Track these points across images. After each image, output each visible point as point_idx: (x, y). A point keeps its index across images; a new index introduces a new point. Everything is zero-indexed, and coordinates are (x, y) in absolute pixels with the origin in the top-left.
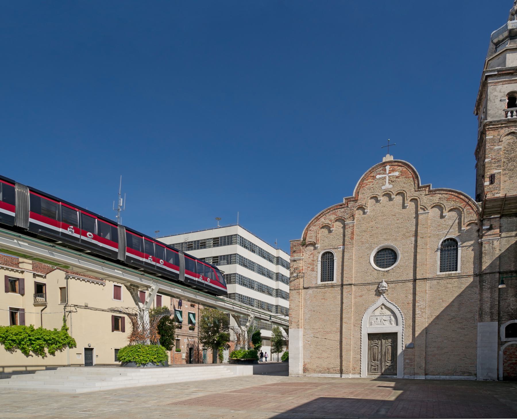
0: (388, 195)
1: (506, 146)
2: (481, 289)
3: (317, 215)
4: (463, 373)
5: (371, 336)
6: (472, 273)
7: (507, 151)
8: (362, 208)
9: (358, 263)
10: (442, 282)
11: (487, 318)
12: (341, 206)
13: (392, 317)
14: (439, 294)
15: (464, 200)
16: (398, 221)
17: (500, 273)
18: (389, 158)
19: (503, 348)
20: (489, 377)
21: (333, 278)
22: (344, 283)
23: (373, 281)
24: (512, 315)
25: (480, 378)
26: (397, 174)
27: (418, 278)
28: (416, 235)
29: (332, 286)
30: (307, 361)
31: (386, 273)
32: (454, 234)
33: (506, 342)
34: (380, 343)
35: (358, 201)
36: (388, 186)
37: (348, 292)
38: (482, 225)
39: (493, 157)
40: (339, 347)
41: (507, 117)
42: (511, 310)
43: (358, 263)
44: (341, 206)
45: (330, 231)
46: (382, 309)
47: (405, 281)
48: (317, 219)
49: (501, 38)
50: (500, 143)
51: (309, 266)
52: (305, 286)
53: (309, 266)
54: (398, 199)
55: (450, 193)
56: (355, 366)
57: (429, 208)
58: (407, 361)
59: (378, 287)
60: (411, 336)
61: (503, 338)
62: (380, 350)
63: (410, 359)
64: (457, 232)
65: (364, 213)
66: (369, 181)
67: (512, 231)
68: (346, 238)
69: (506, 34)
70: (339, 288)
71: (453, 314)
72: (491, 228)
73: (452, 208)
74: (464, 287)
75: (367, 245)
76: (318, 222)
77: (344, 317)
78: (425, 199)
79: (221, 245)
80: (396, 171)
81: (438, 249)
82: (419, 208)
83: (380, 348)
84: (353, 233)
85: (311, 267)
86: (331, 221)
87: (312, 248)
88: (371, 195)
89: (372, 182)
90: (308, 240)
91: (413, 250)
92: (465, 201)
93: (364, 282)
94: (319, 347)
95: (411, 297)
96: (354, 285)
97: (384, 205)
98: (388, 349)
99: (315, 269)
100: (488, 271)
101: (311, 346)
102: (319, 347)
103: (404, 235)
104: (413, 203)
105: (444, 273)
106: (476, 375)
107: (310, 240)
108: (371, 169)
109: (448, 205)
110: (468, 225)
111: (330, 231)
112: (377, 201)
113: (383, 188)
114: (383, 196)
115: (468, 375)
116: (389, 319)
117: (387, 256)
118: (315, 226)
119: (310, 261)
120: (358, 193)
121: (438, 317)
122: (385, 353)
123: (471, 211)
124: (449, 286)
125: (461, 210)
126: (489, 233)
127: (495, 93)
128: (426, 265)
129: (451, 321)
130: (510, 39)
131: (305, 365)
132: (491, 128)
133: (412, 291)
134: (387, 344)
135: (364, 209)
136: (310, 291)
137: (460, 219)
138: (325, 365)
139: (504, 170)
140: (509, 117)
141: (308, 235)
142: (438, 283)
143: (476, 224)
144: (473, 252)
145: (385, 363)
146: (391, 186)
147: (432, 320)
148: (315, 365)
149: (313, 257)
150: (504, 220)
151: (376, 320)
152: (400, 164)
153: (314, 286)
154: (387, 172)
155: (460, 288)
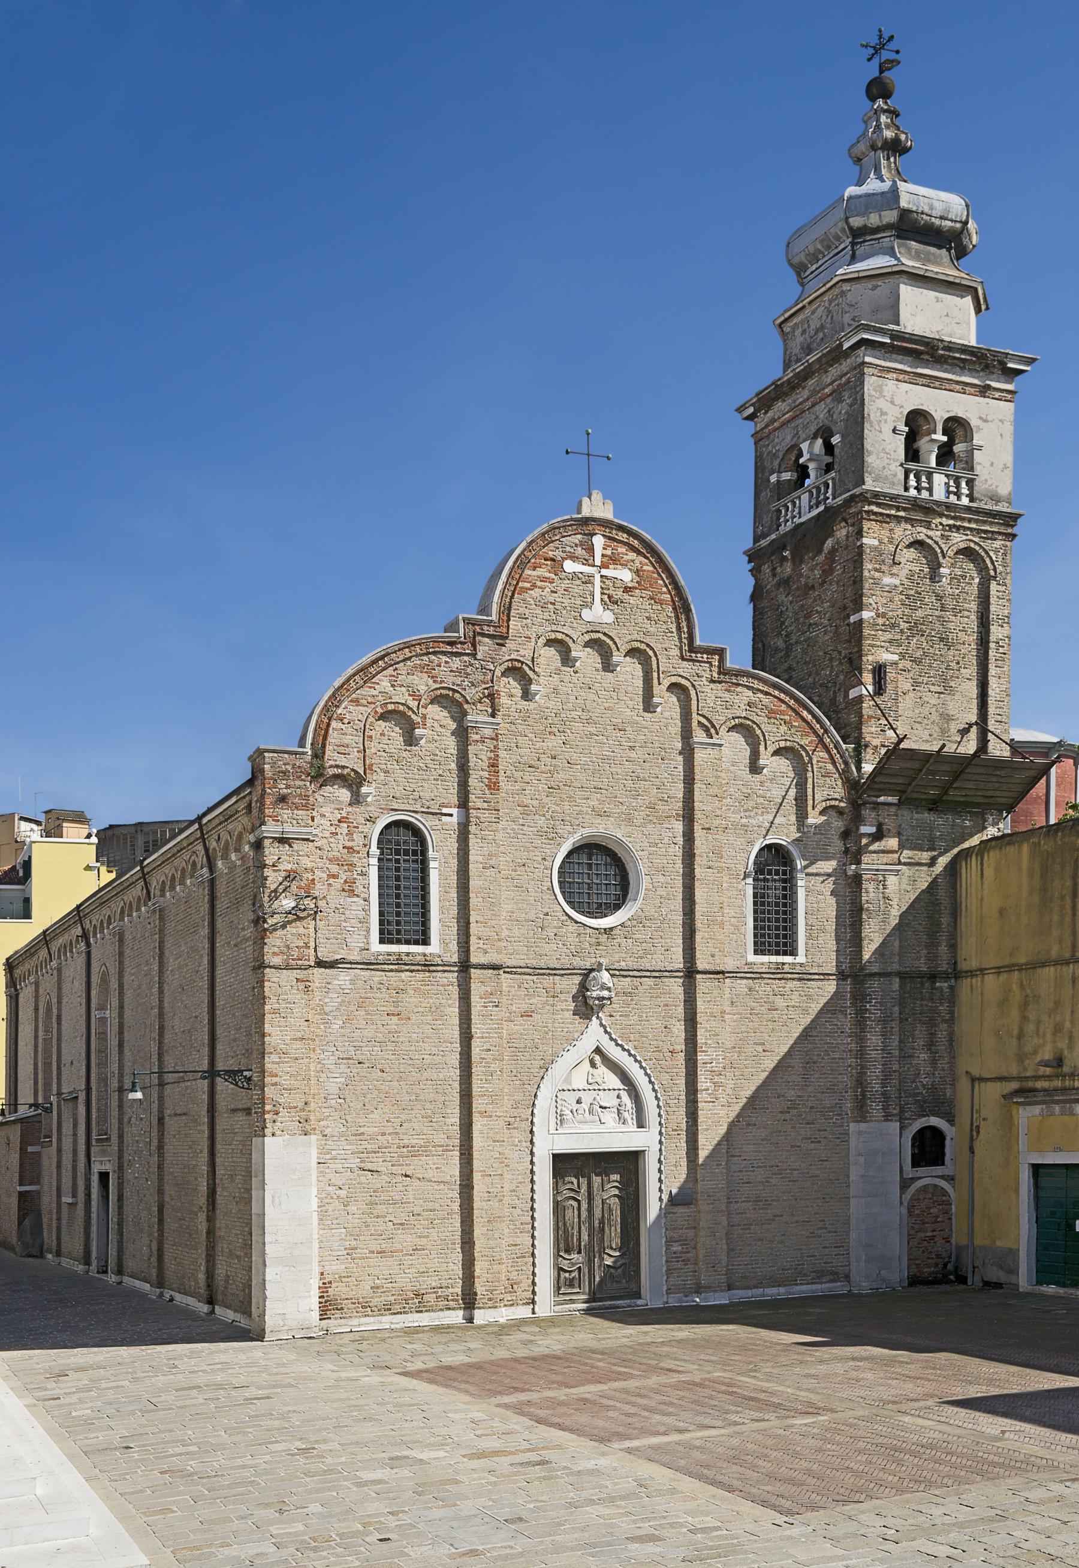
0: (601, 646)
1: (906, 582)
2: (860, 1022)
3: (365, 660)
4: (819, 1275)
5: (563, 1164)
6: (831, 968)
7: (908, 597)
8: (517, 671)
10: (763, 988)
11: (875, 1109)
12: (451, 644)
13: (626, 1099)
14: (761, 1021)
15: (812, 728)
16: (633, 754)
17: (903, 976)
19: (908, 1195)
20: (883, 1280)
21: (391, 942)
22: (474, 960)
23: (566, 962)
24: (925, 1102)
25: (863, 1285)
26: (626, 576)
27: (701, 965)
28: (688, 815)
29: (427, 966)
30: (335, 1268)
31: (603, 938)
32: (785, 835)
33: (913, 1180)
34: (584, 1189)
35: (510, 644)
36: (598, 614)
38: (857, 820)
39: (881, 610)
40: (456, 1207)
41: (906, 489)
42: (921, 1090)
44: (451, 644)
45: (410, 740)
46: (593, 1065)
47: (659, 974)
49: (874, 220)
50: (895, 570)
51: (334, 869)
52: (324, 954)
53: (334, 869)
54: (630, 670)
55: (776, 693)
56: (514, 1275)
57: (723, 731)
58: (676, 1248)
59: (583, 987)
60: (684, 1163)
61: (909, 1172)
62: (584, 1214)
63: (684, 1242)
64: (794, 829)
65: (527, 695)
66: (539, 572)
67: (921, 849)
68: (473, 782)
69: (890, 216)
70: (453, 977)
71: (791, 1094)
72: (878, 836)
73: (782, 744)
74: (815, 1007)
75: (542, 822)
78: (711, 698)
81: (746, 876)
82: (694, 724)
83: (584, 1206)
85: (343, 876)
87: (344, 795)
88: (546, 631)
90: (332, 756)
91: (679, 867)
92: (815, 732)
93: (534, 963)
94: (381, 1209)
95: (679, 1030)
96: (511, 970)
97: (587, 681)
98: (610, 1210)
100: (875, 969)
101: (352, 1208)
103: (652, 807)
104: (674, 699)
105: (765, 959)
106: (847, 1277)
108: (544, 527)
109: (775, 733)
110: (822, 813)
111: (410, 740)
112: (567, 659)
114: (587, 644)
115: (831, 1281)
116: (616, 1102)
117: (598, 874)
118: (356, 702)
119: (337, 848)
120: (507, 611)
121: (752, 1100)
122: (602, 1222)
123: (830, 767)
124: (780, 1002)
125: (806, 759)
126: (875, 847)
127: (881, 403)
128: (722, 924)
129: (788, 1116)
130: (899, 237)
131: (324, 1287)
132: (875, 514)
133: (681, 1010)
134: (608, 1189)
135: (530, 681)
136: (342, 978)
137: (801, 786)
138: (406, 1281)
139: (903, 656)
140: (913, 492)
141: (333, 738)
142: (750, 989)
143: (840, 812)
144: (832, 901)
145: (602, 1259)
146: (608, 617)
147: (737, 1108)
148: (366, 1286)
150: (907, 816)
151: (575, 1106)
152: (636, 543)
153: (355, 956)
155: (805, 1011)
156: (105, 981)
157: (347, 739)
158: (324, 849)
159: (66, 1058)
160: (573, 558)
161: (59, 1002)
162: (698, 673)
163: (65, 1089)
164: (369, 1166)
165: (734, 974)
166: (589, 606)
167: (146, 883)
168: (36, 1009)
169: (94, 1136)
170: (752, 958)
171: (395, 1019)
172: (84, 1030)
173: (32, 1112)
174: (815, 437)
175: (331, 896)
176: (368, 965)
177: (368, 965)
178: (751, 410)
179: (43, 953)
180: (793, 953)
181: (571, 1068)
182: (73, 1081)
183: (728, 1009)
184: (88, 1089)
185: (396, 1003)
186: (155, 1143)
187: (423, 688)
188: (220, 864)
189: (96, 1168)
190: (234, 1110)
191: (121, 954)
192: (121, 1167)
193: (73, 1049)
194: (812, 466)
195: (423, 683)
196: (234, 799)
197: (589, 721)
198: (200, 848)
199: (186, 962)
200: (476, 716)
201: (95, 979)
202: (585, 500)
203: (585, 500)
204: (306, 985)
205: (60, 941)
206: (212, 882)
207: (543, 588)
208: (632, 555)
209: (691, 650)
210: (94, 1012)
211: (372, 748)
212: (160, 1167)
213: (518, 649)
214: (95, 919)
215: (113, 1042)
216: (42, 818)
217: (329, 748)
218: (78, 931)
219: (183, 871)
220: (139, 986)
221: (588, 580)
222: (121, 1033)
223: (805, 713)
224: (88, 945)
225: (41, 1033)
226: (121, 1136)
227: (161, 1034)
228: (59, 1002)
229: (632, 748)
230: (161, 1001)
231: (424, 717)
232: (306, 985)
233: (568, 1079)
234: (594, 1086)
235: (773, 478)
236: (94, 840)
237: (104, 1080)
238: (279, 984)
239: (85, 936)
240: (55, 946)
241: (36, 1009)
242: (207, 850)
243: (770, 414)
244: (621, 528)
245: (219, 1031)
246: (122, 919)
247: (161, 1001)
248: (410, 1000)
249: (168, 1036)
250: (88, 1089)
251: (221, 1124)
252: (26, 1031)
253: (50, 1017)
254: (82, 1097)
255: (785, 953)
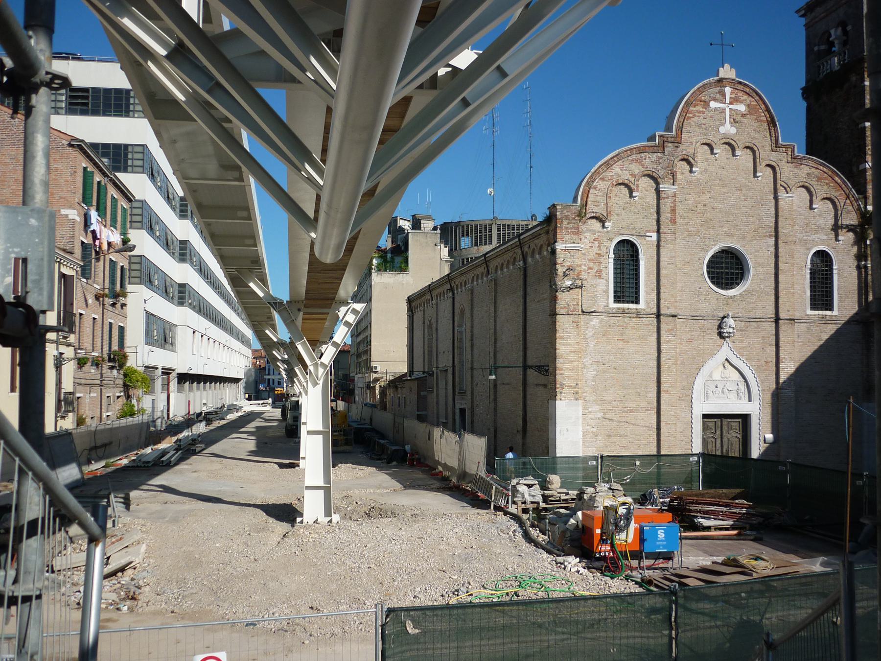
9: (679, 271)
18: (727, 72)
22: (662, 312)
26: (742, 108)
29: (638, 314)
31: (730, 301)
35: (682, 147)
36: (728, 129)
37: (669, 330)
43: (679, 271)
47: (760, 320)
48: (608, 165)
53: (591, 265)
59: (720, 327)
62: (718, 445)
68: (662, 219)
76: (608, 174)
77: (663, 379)
78: (787, 171)
79: (95, 113)
80: (741, 102)
82: (778, 186)
83: (719, 441)
84: (673, 210)
85: (596, 269)
86: (634, 176)
87: (597, 225)
89: (704, 113)
94: (614, 439)
97: (722, 164)
99: (604, 274)
102: (614, 439)
105: (816, 312)
107: (596, 209)
109: (821, 190)
113: (722, 130)
117: (727, 268)
118: (603, 179)
120: (680, 130)
128: (793, 294)
141: (591, 198)
142: (808, 329)
146: (733, 131)
149: (599, 247)
151: (715, 389)
152: (748, 90)
154: (728, 101)
156: (462, 313)
157: (598, 198)
158: (585, 254)
159: (441, 350)
160: (715, 100)
161: (437, 321)
162: (781, 159)
163: (441, 365)
164: (607, 416)
165: (800, 321)
166: (723, 124)
167: (487, 266)
168: (424, 324)
169: (457, 391)
170: (809, 312)
171: (621, 342)
172: (451, 336)
173: (421, 375)
174: (837, 27)
175: (589, 279)
176: (609, 313)
177: (609, 313)
178: (803, 12)
179: (428, 296)
180: (831, 309)
181: (714, 369)
182: (445, 361)
183: (796, 339)
184: (454, 366)
185: (622, 334)
186: (492, 397)
187: (637, 171)
188: (530, 260)
189: (458, 406)
190: (537, 385)
191: (472, 300)
192: (472, 407)
193: (445, 344)
194: (836, 42)
195: (637, 169)
196: (539, 228)
197: (724, 186)
198: (518, 251)
199: (509, 308)
200: (664, 187)
201: (457, 311)
202: (721, 69)
203: (721, 69)
204: (577, 324)
205: (438, 291)
206: (525, 269)
207: (699, 117)
208: (746, 97)
209: (776, 146)
210: (456, 328)
211: (611, 202)
212: (495, 409)
213: (685, 149)
214: (458, 281)
215: (468, 345)
216: (411, 219)
217: (589, 203)
218: (448, 286)
219: (508, 261)
220: (482, 317)
221: (723, 111)
222: (472, 340)
223: (837, 179)
224: (453, 294)
225: (426, 336)
226: (472, 392)
227: (495, 342)
228: (437, 321)
229: (745, 200)
230: (495, 326)
231: (638, 186)
232: (577, 324)
233: (710, 376)
234: (725, 379)
235: (816, 49)
236: (439, 231)
237: (461, 362)
238: (563, 322)
239: (452, 289)
240: (434, 293)
241: (424, 324)
242: (522, 252)
243: (813, 14)
244: (740, 83)
245: (528, 345)
246: (472, 282)
247: (495, 326)
248: (629, 332)
249: (499, 344)
250: (454, 366)
251: (530, 391)
252: (418, 333)
253: (431, 328)
254: (450, 370)
255: (827, 310)
